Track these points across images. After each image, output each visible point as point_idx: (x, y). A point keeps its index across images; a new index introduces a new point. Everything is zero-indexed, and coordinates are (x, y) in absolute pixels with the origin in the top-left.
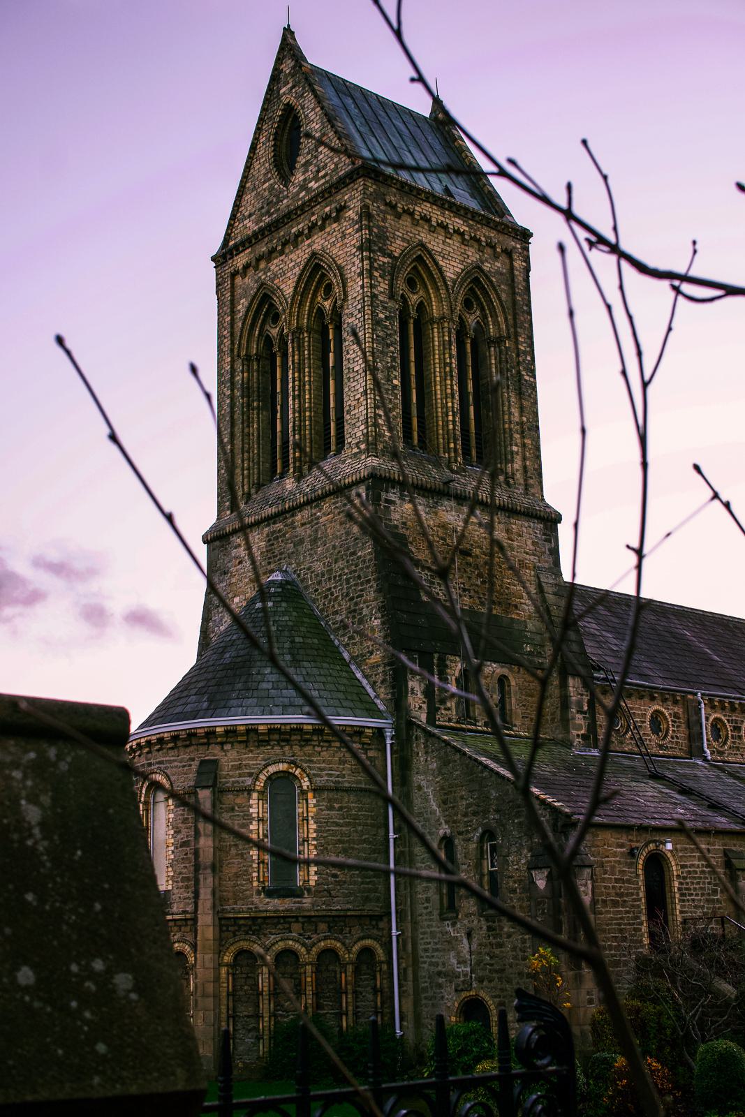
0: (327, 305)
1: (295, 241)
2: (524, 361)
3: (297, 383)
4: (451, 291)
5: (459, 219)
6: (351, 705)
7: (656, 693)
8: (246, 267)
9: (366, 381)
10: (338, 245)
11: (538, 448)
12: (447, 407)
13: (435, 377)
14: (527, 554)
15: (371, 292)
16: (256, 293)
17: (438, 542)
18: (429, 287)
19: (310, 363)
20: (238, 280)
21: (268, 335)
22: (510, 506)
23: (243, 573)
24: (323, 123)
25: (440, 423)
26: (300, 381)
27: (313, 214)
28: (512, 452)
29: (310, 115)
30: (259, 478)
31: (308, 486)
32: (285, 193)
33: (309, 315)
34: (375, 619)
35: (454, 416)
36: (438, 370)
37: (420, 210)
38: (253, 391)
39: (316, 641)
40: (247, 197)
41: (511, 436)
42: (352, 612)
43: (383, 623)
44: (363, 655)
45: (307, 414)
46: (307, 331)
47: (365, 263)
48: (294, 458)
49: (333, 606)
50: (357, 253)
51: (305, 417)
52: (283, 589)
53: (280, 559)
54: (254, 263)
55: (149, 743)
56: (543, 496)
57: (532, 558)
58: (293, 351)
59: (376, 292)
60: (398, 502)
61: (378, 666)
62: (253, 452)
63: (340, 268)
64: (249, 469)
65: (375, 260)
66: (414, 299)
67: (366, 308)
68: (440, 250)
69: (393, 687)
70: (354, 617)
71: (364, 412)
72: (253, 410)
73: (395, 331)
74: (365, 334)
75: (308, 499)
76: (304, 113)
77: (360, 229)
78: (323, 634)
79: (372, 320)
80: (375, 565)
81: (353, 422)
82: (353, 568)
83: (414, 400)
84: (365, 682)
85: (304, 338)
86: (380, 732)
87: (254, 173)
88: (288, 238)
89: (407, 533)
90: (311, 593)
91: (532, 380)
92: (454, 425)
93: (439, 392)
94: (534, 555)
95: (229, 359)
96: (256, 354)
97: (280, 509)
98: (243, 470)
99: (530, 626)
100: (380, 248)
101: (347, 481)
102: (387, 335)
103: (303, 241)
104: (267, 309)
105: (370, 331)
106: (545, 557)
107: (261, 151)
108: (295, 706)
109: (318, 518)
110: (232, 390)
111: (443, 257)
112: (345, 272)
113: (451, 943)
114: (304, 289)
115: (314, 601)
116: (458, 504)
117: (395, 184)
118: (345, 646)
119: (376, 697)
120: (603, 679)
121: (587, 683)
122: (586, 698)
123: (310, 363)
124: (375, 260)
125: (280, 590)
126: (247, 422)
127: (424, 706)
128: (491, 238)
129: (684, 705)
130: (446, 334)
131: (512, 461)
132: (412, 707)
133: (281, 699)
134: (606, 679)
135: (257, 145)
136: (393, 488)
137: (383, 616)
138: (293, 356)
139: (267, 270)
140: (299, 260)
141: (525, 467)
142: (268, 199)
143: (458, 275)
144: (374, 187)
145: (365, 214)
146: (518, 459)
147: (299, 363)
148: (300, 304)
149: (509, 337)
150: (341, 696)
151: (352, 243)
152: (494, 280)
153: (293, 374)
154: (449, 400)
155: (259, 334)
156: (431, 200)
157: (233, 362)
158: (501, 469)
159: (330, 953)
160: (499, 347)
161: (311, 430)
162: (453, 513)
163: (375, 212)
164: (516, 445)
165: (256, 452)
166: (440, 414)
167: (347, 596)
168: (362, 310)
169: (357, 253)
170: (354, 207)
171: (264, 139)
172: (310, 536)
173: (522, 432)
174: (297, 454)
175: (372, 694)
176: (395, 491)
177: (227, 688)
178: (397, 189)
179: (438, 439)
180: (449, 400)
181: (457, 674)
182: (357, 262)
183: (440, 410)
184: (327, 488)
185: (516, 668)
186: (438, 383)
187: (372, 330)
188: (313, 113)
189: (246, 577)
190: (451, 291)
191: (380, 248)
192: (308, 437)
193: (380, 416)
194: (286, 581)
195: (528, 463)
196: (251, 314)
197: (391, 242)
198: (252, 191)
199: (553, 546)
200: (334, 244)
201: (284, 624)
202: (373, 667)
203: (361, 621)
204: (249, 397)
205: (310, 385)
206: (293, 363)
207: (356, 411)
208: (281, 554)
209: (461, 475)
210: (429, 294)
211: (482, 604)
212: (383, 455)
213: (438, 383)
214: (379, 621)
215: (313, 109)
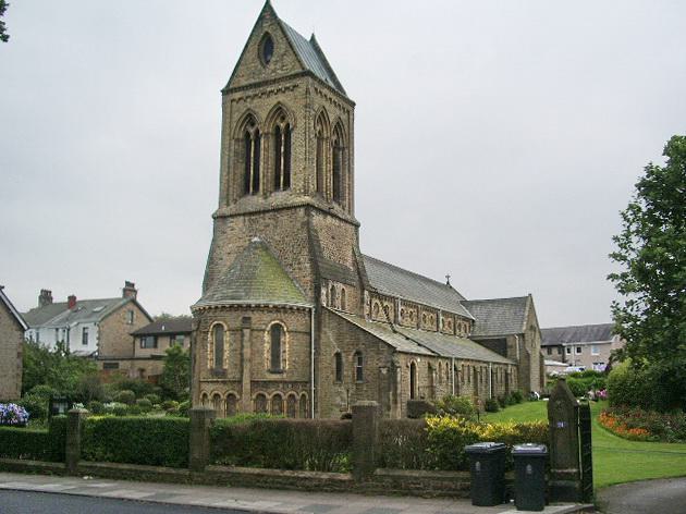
8: (240, 99)
40: (240, 67)
55: (216, 308)
63: (293, 112)
86: (310, 309)
113: (339, 393)
145: (307, 91)
159: (292, 396)
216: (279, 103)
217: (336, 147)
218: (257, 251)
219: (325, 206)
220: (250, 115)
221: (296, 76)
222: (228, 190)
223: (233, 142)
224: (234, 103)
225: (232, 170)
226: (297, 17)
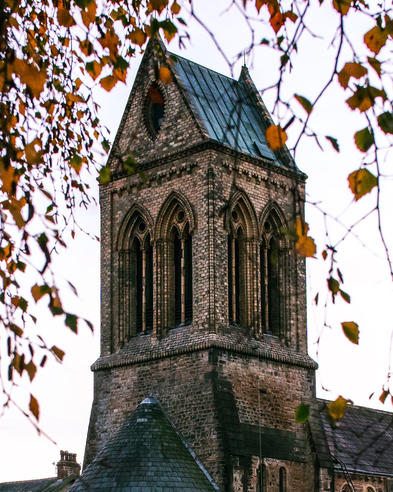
0: (181, 226)
1: (160, 180)
2: (299, 263)
3: (159, 275)
4: (258, 221)
5: (265, 171)
6: (200, 487)
7: (369, 476)
8: (123, 190)
9: (209, 284)
10: (191, 190)
11: (305, 321)
12: (254, 297)
13: (247, 277)
14: (298, 390)
15: (214, 227)
16: (130, 209)
17: (248, 385)
18: (245, 218)
19: (167, 263)
20: (116, 197)
21: (136, 237)
22: (289, 361)
23: (121, 394)
24: (181, 103)
25: (249, 307)
26: (161, 274)
27: (173, 165)
28: (290, 324)
29: (171, 95)
30: (129, 332)
31: (168, 345)
32: (152, 145)
33: (168, 230)
34: (213, 434)
35: (258, 303)
36: (249, 272)
37: (243, 168)
38: (126, 275)
39: (175, 445)
41: (290, 314)
42: (198, 428)
43: (218, 438)
44: (204, 455)
45: (166, 296)
46: (166, 242)
47: (210, 207)
48: (157, 324)
49: (185, 423)
50: (205, 200)
51: (164, 298)
52: (152, 410)
53: (148, 389)
54: (129, 188)
56: (307, 352)
57: (300, 392)
58: (157, 254)
59: (216, 226)
60: (227, 362)
61: (214, 463)
62: (126, 314)
63: (192, 206)
64: (123, 326)
65: (216, 205)
66: (236, 225)
67: (210, 237)
68: (252, 193)
69: (224, 476)
70: (199, 432)
71: (208, 304)
72: (126, 286)
73: (226, 250)
74: (209, 254)
75: (168, 354)
76: (167, 92)
77: (207, 184)
78: (178, 440)
79: (214, 245)
80: (214, 402)
81: (200, 309)
82: (199, 401)
83: (234, 293)
84: (205, 472)
85: (164, 246)
87: (129, 125)
88: (154, 177)
89: (231, 381)
90: (169, 413)
91: (304, 276)
92: (258, 309)
93: (249, 287)
94: (302, 391)
95: (110, 251)
96: (128, 250)
97: (149, 357)
98: (119, 326)
99: (298, 436)
100: (219, 196)
101: (196, 347)
102: (222, 254)
103: (165, 181)
104: (137, 220)
105: (213, 252)
106: (307, 392)
107: (134, 110)
108: (169, 487)
109: (175, 367)
110: (112, 272)
111: (254, 198)
112: (196, 209)
114: (166, 214)
115: (172, 418)
116: (260, 361)
117: (228, 152)
118: (193, 448)
119: (212, 481)
120: (340, 469)
121: (331, 472)
122: (329, 481)
123: (167, 263)
124: (216, 205)
125: (150, 411)
126: (121, 295)
127: (242, 488)
128: (282, 182)
129: (385, 483)
130: (255, 249)
131: (290, 330)
132: (235, 489)
133: (161, 482)
134: (342, 469)
135: (131, 105)
136: (224, 353)
137: (218, 433)
138: (157, 257)
139: (138, 195)
140: (162, 194)
141: (297, 334)
142: (139, 146)
143: (263, 209)
144: (216, 155)
145: (210, 174)
146: (294, 329)
147: (161, 262)
148: (162, 223)
149: (291, 248)
150: (193, 480)
151: (201, 192)
152: (283, 210)
153: (157, 269)
154: (255, 293)
155: (130, 237)
156: (248, 160)
157: (112, 252)
158: (283, 335)
160: (285, 255)
161: (168, 306)
162: (257, 367)
163: (216, 172)
164: (293, 320)
165: (128, 314)
166: (249, 302)
167: (194, 418)
168: (208, 238)
169: (205, 200)
170: (203, 168)
171: (136, 102)
172: (169, 377)
173: (297, 311)
174: (159, 322)
175: (210, 480)
176: (225, 355)
177: (127, 474)
178: (229, 155)
179: (247, 317)
180: (255, 293)
181: (257, 467)
182: (205, 205)
183: (249, 299)
184: (182, 350)
185: (290, 462)
186: (249, 281)
187: (214, 251)
188: (173, 94)
189: (122, 397)
190: (258, 221)
191: (219, 196)
192: (166, 311)
193: (217, 307)
194: (153, 404)
195: (299, 331)
196: (126, 223)
197: (225, 191)
198: (127, 138)
199: (312, 384)
200: (187, 188)
201: (156, 433)
202: (211, 463)
203: (203, 435)
204: (123, 278)
205: (167, 277)
206: (157, 262)
207: (202, 303)
208: (149, 386)
209: (261, 341)
210: (245, 222)
211: (272, 423)
212: (219, 332)
213: (249, 281)
214: (216, 436)
215: (174, 91)
216: (173, 193)
219: (246, 344)
220: (136, 214)
222: (112, 328)
223: (116, 256)
225: (116, 298)
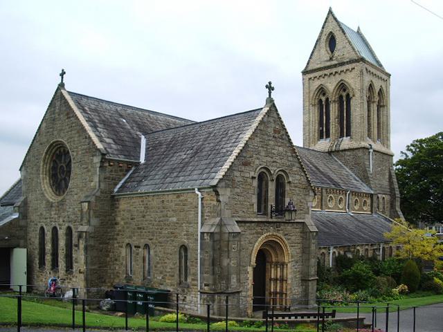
217: (379, 106)
218: (188, 298)
221: (351, 62)
224: (311, 81)
226: (349, 20)
